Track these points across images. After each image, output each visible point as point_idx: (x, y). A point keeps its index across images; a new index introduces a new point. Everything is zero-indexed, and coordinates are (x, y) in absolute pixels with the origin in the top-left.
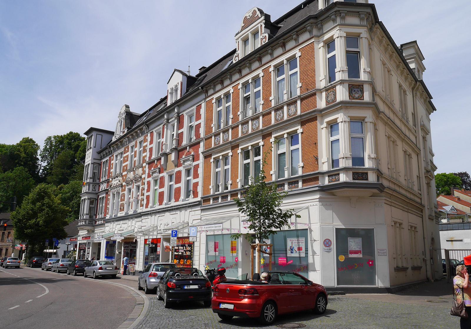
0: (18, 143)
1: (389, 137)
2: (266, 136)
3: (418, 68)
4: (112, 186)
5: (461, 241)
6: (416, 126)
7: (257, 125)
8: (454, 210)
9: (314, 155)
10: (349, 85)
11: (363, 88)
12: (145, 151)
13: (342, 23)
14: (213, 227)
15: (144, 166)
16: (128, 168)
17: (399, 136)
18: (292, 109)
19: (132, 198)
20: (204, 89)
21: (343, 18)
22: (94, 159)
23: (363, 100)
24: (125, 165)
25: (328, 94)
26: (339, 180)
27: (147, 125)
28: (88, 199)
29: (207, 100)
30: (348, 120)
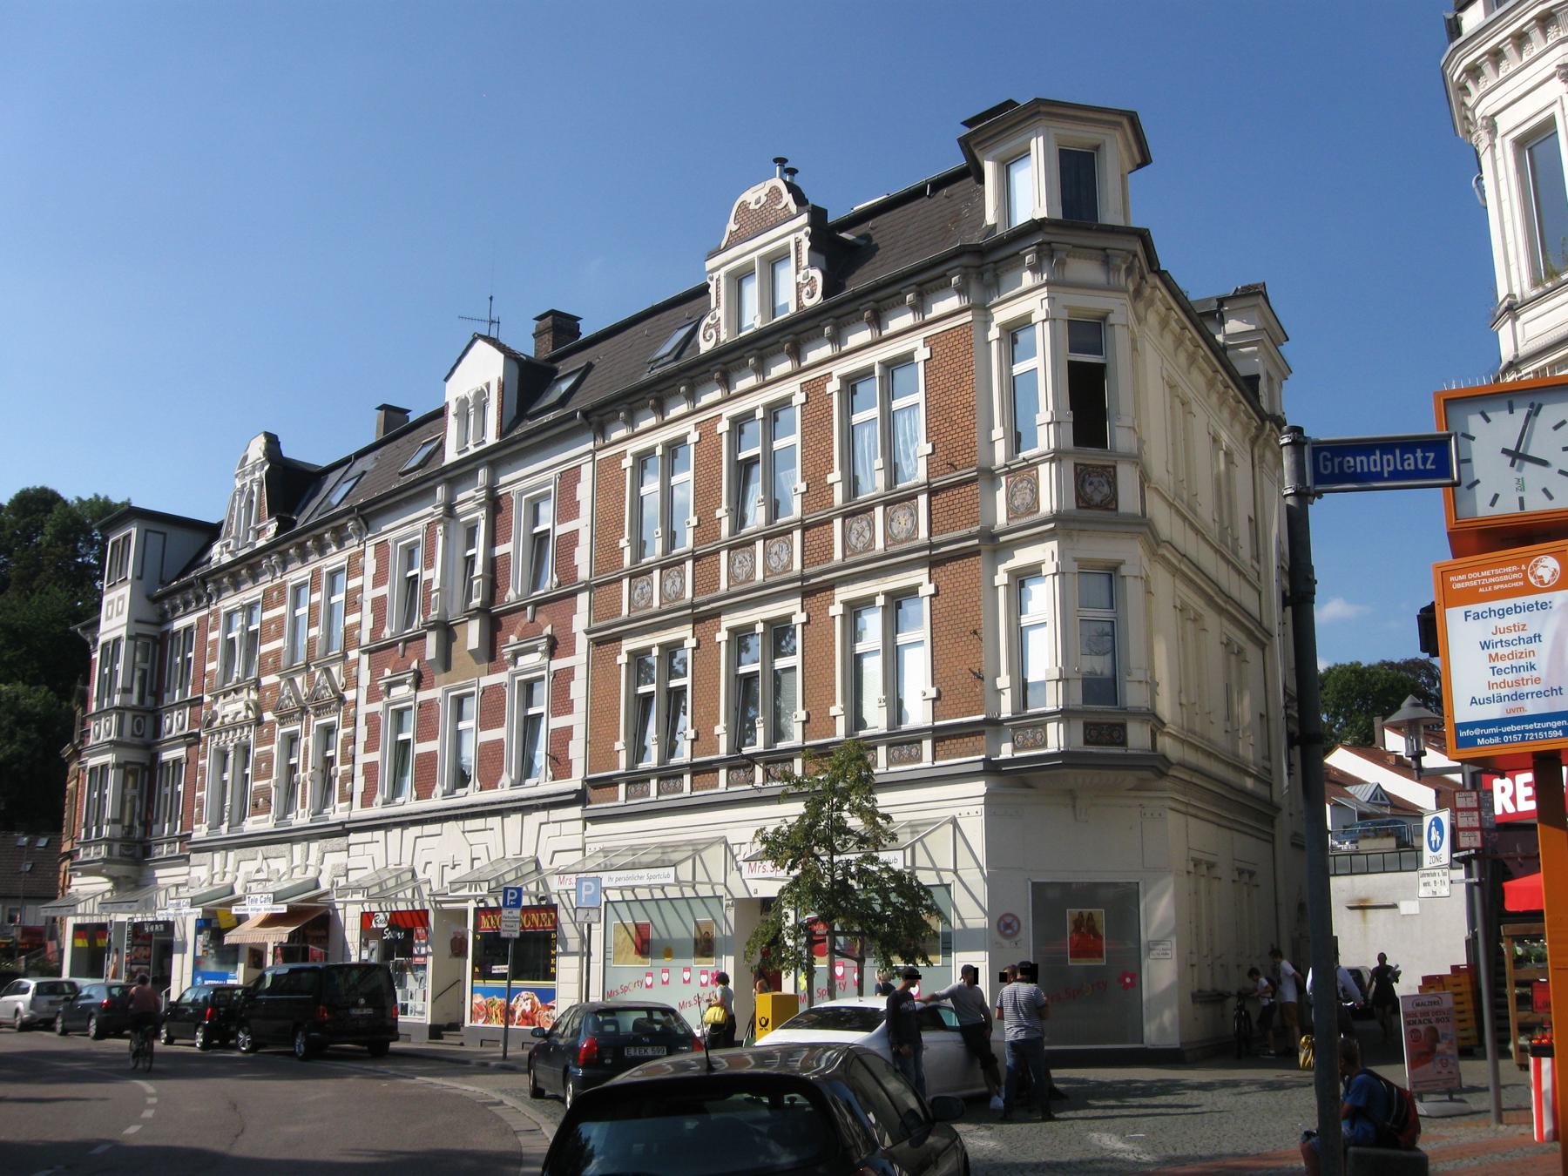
1: (1182, 609)
2: (812, 590)
3: (1268, 373)
4: (217, 724)
5: (1394, 906)
6: (1262, 558)
7: (785, 558)
8: (1382, 799)
9: (971, 666)
10: (1076, 465)
12: (352, 604)
14: (641, 878)
15: (354, 661)
16: (284, 662)
17: (1210, 601)
18: (903, 523)
19: (305, 769)
20: (595, 419)
22: (137, 621)
24: (271, 652)
25: (1016, 486)
26: (1044, 745)
27: (362, 516)
28: (118, 766)
29: (600, 456)
30: (1074, 567)
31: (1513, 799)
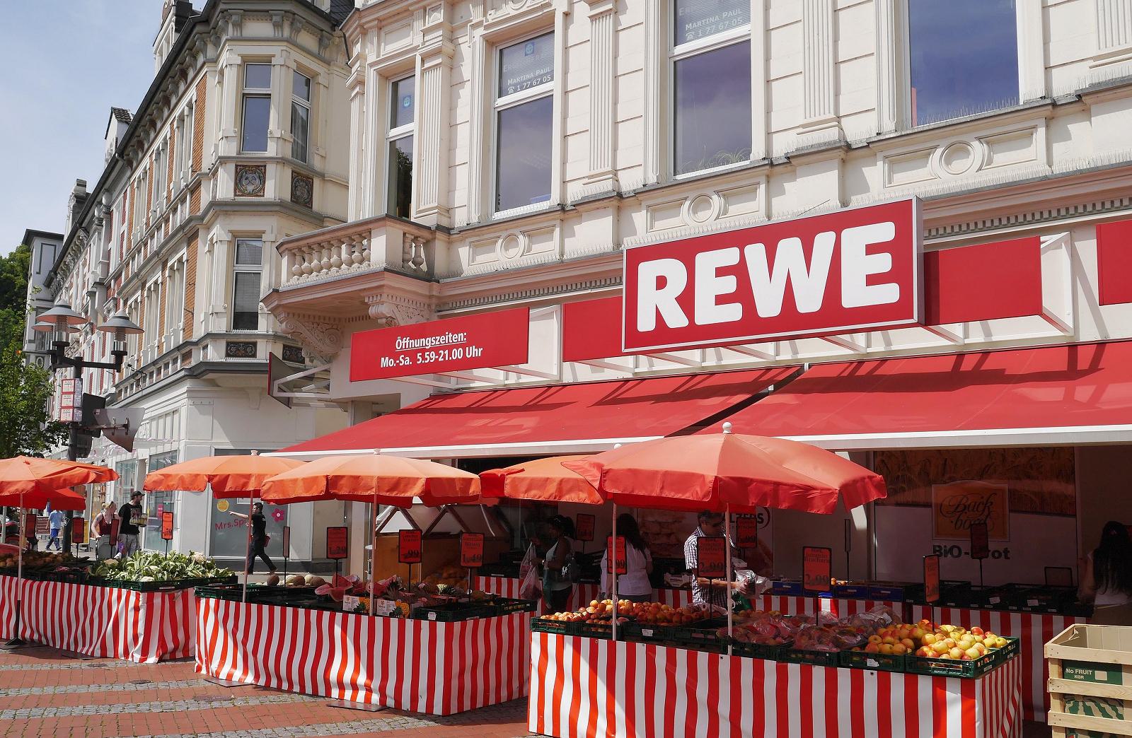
0: (12, 253)
11: (265, 172)
13: (235, 34)
21: (238, 25)
23: (263, 196)
31: (687, 301)
